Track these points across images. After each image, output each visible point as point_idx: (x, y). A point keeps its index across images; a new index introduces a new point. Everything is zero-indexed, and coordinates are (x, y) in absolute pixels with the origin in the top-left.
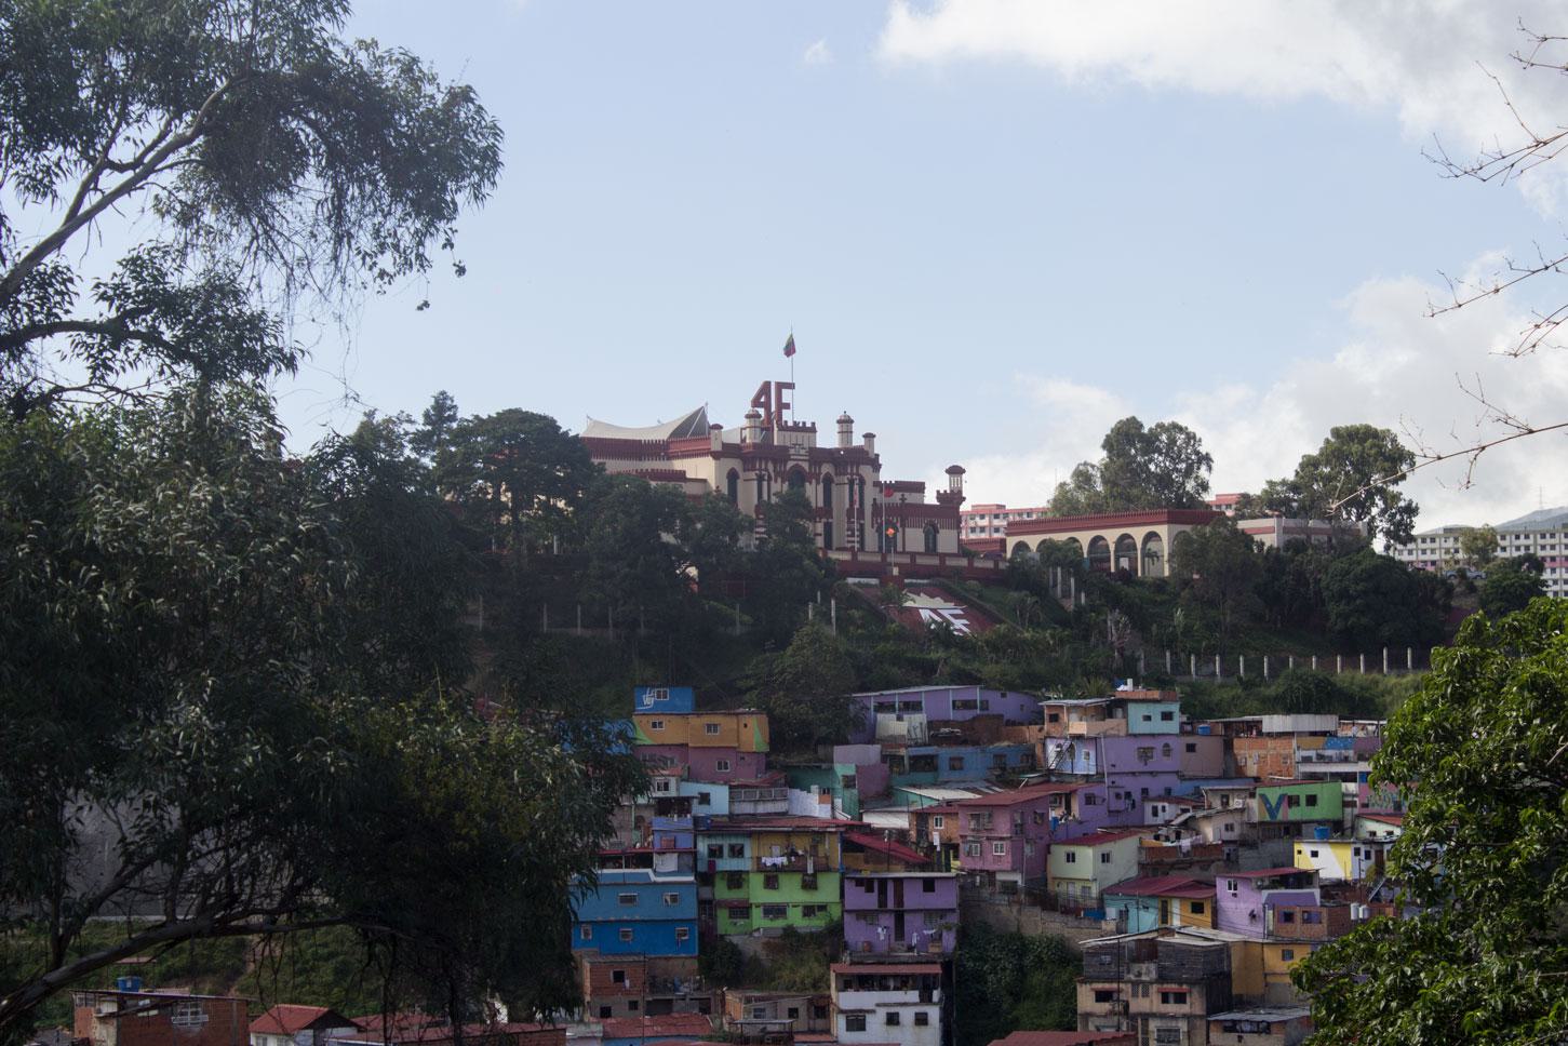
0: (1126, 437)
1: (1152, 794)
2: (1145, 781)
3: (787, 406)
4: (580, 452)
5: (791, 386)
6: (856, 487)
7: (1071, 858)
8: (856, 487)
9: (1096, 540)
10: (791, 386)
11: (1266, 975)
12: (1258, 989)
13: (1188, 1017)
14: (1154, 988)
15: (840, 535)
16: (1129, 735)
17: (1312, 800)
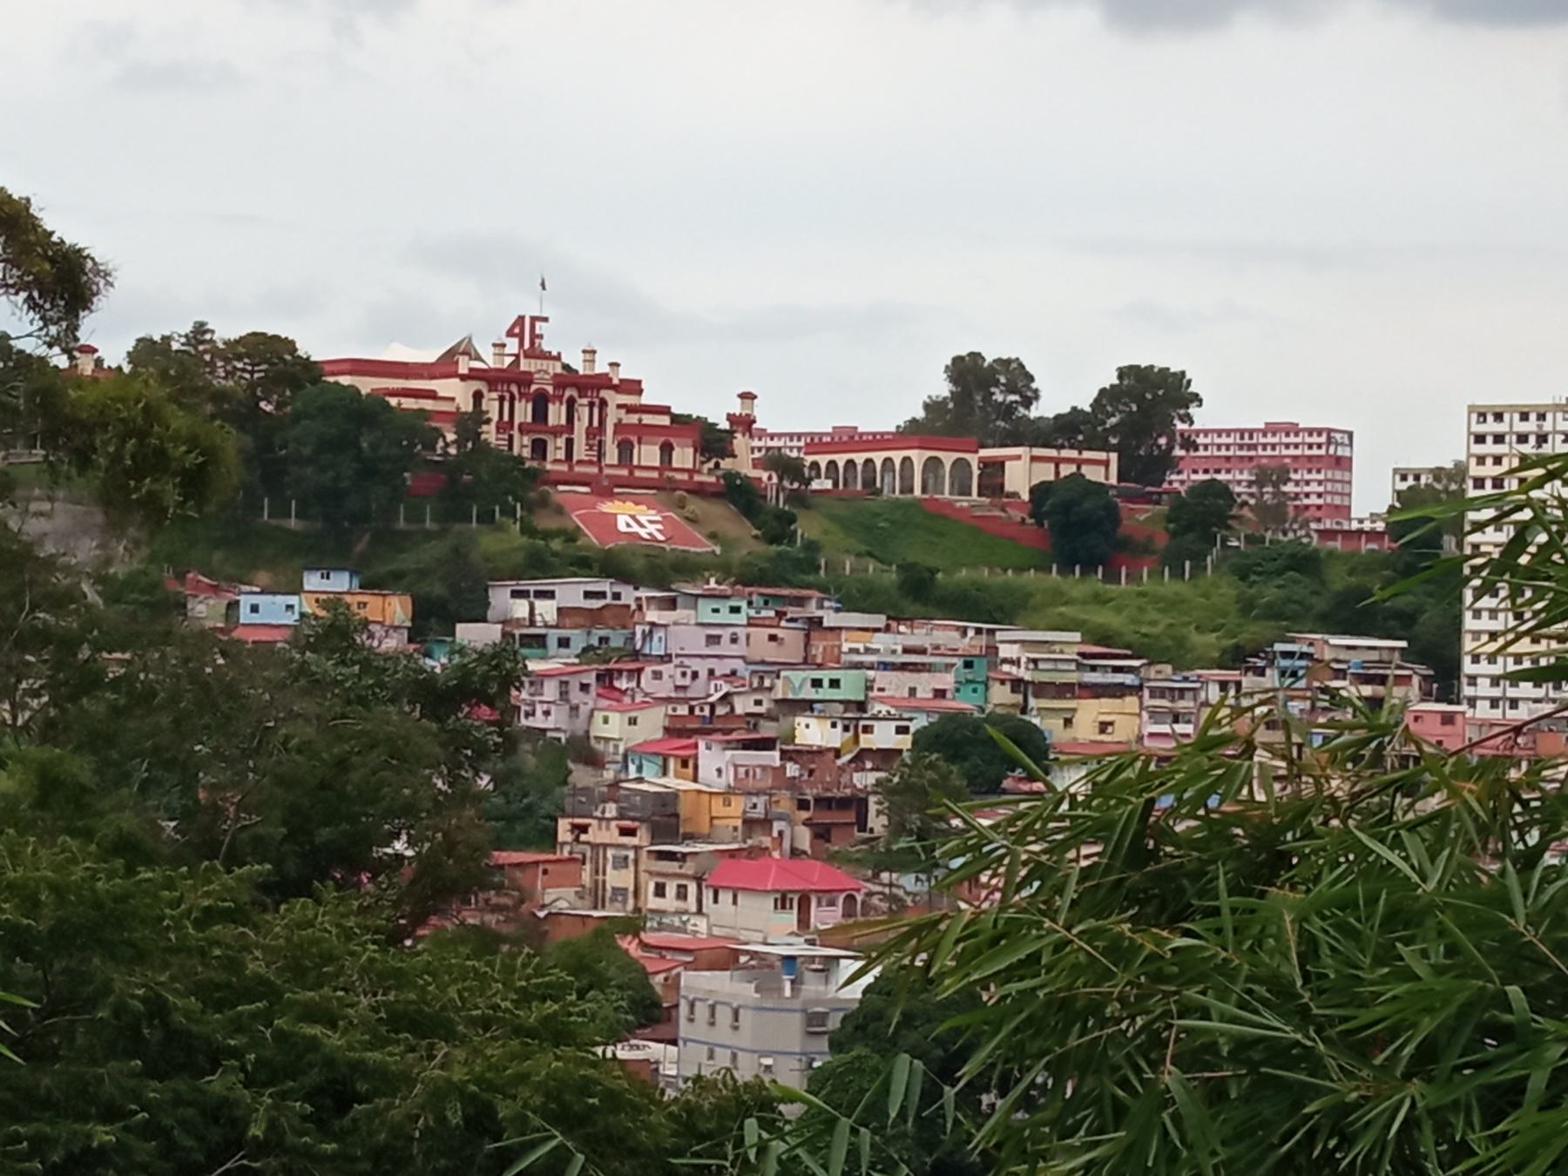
0: (969, 373)
1: (718, 673)
2: (712, 663)
3: (541, 337)
4: (311, 371)
5: (546, 320)
6: (596, 411)
7: (606, 721)
8: (596, 411)
9: (869, 461)
10: (546, 320)
11: (712, 818)
12: (705, 829)
13: (637, 848)
14: (613, 824)
15: (580, 451)
16: (699, 624)
17: (835, 683)
